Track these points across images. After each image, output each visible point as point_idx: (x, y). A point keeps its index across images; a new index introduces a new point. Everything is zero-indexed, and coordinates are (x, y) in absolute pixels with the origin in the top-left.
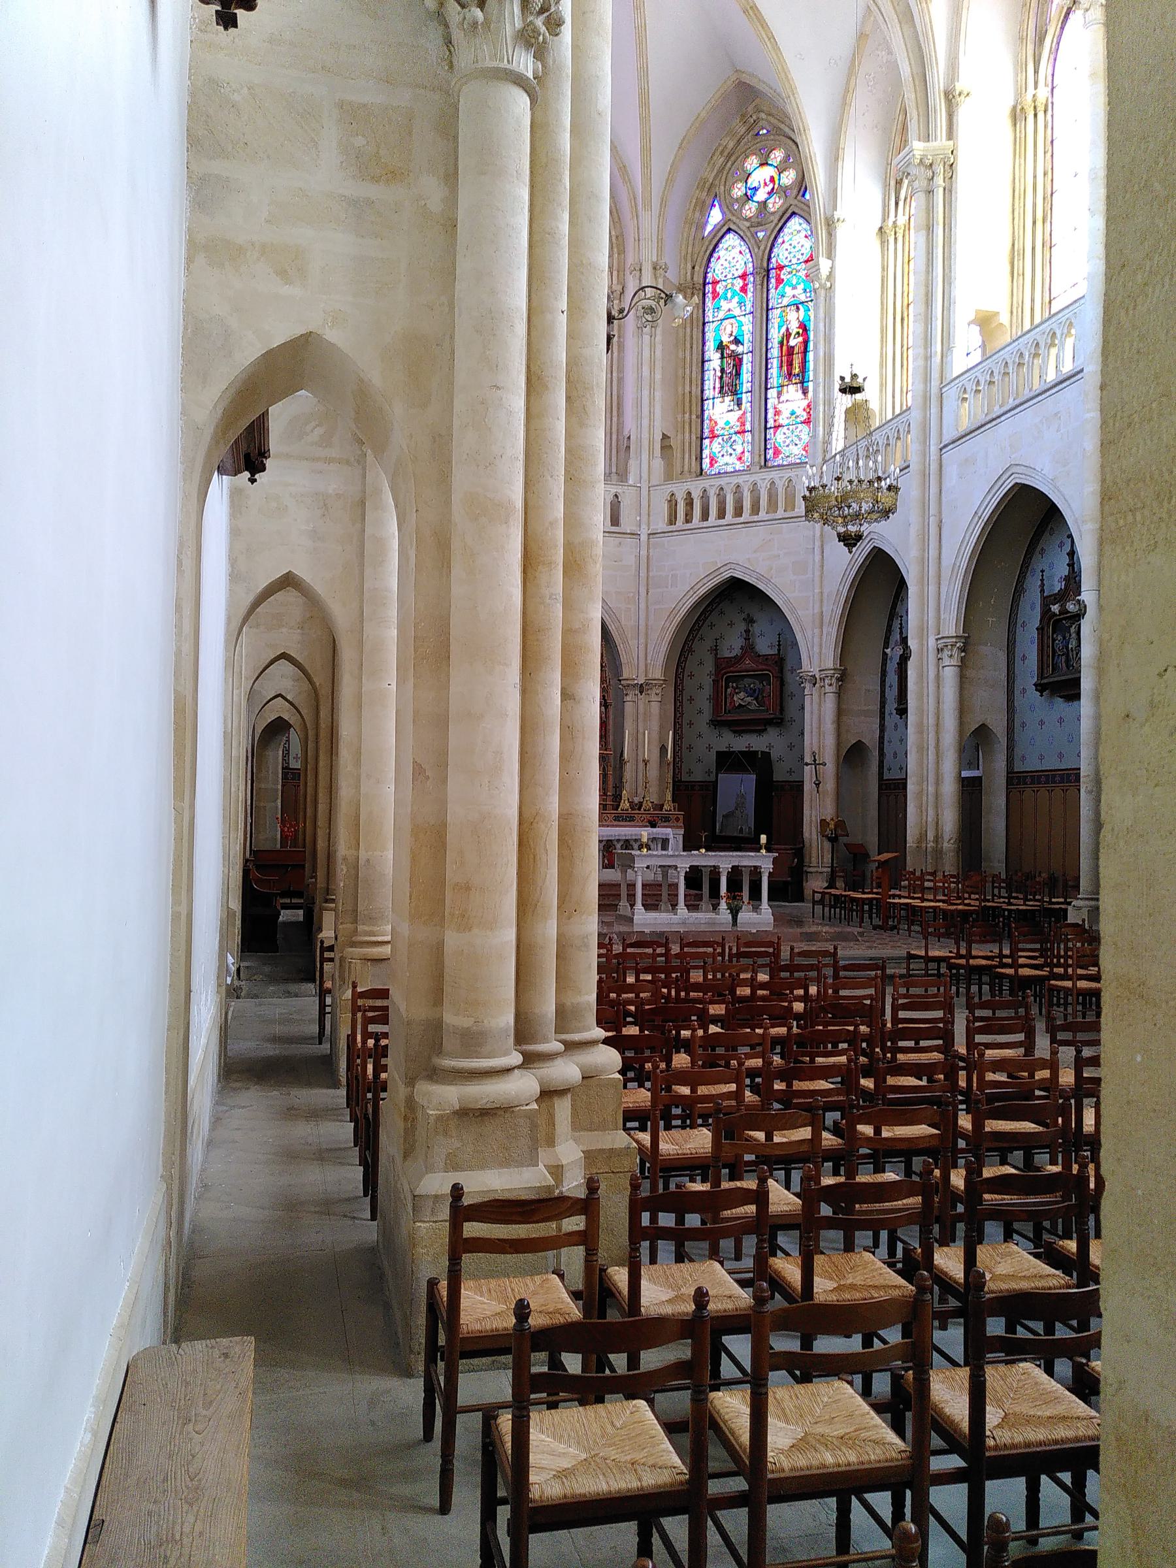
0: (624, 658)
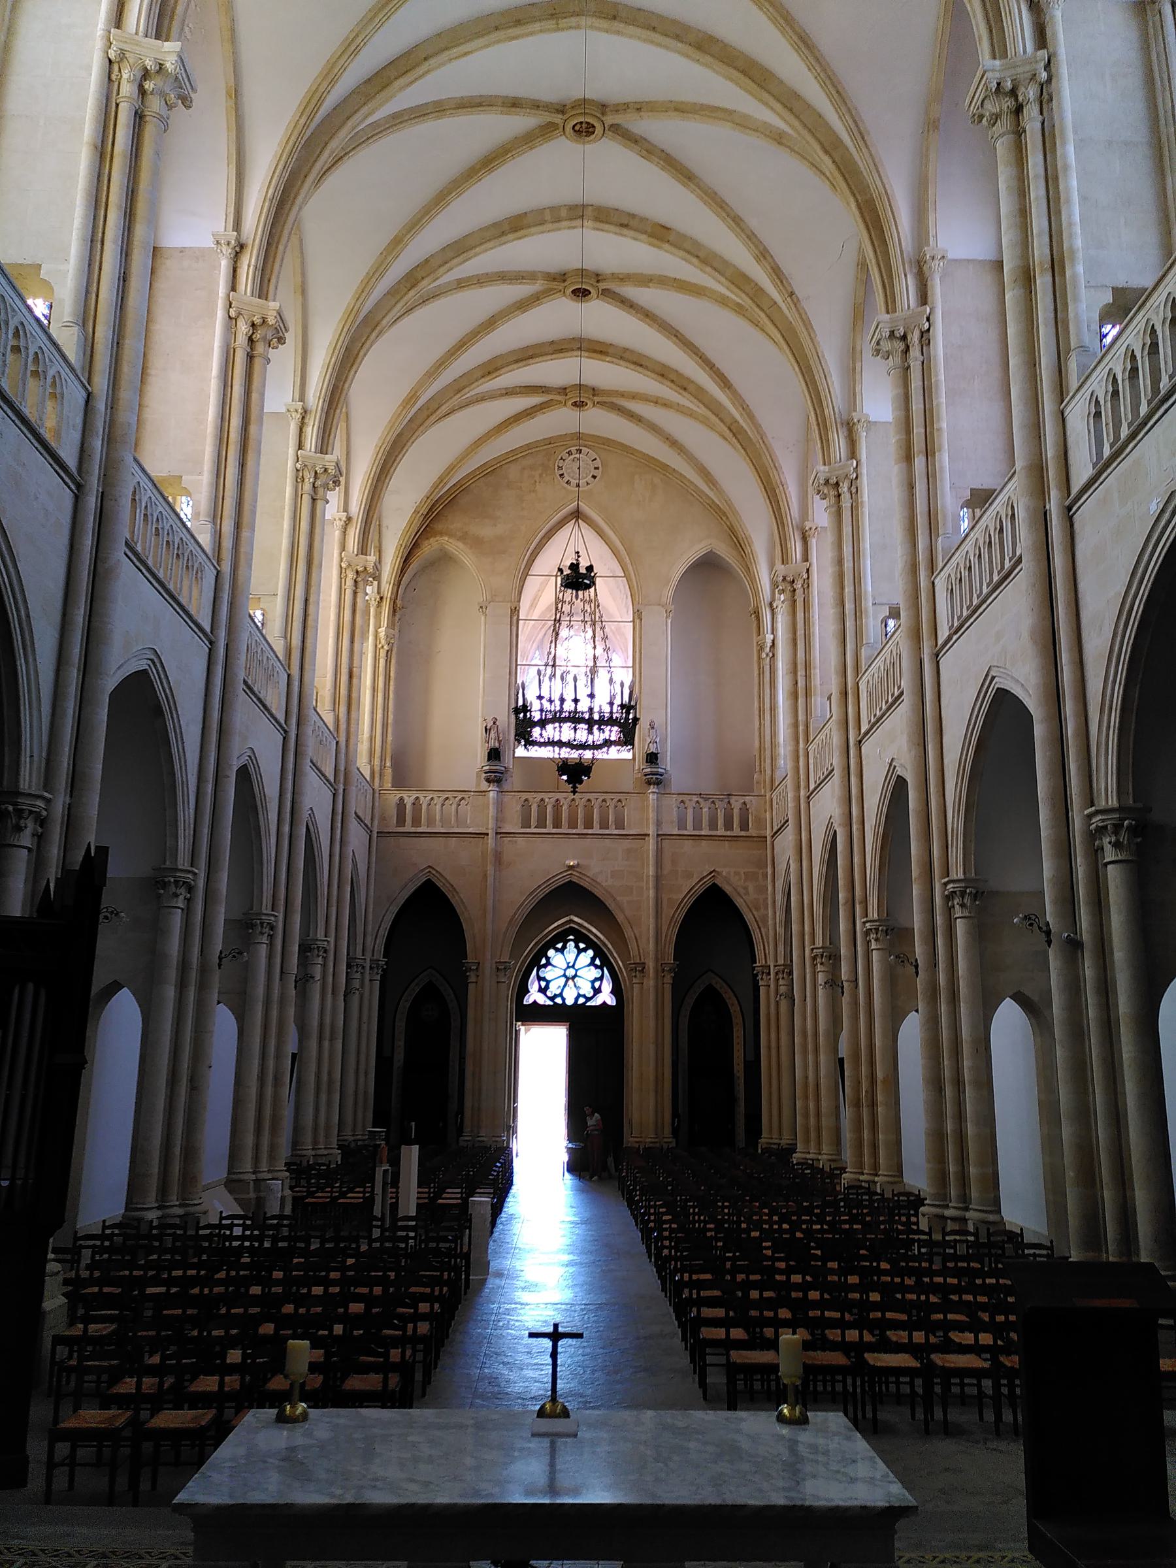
0: (620, 918)
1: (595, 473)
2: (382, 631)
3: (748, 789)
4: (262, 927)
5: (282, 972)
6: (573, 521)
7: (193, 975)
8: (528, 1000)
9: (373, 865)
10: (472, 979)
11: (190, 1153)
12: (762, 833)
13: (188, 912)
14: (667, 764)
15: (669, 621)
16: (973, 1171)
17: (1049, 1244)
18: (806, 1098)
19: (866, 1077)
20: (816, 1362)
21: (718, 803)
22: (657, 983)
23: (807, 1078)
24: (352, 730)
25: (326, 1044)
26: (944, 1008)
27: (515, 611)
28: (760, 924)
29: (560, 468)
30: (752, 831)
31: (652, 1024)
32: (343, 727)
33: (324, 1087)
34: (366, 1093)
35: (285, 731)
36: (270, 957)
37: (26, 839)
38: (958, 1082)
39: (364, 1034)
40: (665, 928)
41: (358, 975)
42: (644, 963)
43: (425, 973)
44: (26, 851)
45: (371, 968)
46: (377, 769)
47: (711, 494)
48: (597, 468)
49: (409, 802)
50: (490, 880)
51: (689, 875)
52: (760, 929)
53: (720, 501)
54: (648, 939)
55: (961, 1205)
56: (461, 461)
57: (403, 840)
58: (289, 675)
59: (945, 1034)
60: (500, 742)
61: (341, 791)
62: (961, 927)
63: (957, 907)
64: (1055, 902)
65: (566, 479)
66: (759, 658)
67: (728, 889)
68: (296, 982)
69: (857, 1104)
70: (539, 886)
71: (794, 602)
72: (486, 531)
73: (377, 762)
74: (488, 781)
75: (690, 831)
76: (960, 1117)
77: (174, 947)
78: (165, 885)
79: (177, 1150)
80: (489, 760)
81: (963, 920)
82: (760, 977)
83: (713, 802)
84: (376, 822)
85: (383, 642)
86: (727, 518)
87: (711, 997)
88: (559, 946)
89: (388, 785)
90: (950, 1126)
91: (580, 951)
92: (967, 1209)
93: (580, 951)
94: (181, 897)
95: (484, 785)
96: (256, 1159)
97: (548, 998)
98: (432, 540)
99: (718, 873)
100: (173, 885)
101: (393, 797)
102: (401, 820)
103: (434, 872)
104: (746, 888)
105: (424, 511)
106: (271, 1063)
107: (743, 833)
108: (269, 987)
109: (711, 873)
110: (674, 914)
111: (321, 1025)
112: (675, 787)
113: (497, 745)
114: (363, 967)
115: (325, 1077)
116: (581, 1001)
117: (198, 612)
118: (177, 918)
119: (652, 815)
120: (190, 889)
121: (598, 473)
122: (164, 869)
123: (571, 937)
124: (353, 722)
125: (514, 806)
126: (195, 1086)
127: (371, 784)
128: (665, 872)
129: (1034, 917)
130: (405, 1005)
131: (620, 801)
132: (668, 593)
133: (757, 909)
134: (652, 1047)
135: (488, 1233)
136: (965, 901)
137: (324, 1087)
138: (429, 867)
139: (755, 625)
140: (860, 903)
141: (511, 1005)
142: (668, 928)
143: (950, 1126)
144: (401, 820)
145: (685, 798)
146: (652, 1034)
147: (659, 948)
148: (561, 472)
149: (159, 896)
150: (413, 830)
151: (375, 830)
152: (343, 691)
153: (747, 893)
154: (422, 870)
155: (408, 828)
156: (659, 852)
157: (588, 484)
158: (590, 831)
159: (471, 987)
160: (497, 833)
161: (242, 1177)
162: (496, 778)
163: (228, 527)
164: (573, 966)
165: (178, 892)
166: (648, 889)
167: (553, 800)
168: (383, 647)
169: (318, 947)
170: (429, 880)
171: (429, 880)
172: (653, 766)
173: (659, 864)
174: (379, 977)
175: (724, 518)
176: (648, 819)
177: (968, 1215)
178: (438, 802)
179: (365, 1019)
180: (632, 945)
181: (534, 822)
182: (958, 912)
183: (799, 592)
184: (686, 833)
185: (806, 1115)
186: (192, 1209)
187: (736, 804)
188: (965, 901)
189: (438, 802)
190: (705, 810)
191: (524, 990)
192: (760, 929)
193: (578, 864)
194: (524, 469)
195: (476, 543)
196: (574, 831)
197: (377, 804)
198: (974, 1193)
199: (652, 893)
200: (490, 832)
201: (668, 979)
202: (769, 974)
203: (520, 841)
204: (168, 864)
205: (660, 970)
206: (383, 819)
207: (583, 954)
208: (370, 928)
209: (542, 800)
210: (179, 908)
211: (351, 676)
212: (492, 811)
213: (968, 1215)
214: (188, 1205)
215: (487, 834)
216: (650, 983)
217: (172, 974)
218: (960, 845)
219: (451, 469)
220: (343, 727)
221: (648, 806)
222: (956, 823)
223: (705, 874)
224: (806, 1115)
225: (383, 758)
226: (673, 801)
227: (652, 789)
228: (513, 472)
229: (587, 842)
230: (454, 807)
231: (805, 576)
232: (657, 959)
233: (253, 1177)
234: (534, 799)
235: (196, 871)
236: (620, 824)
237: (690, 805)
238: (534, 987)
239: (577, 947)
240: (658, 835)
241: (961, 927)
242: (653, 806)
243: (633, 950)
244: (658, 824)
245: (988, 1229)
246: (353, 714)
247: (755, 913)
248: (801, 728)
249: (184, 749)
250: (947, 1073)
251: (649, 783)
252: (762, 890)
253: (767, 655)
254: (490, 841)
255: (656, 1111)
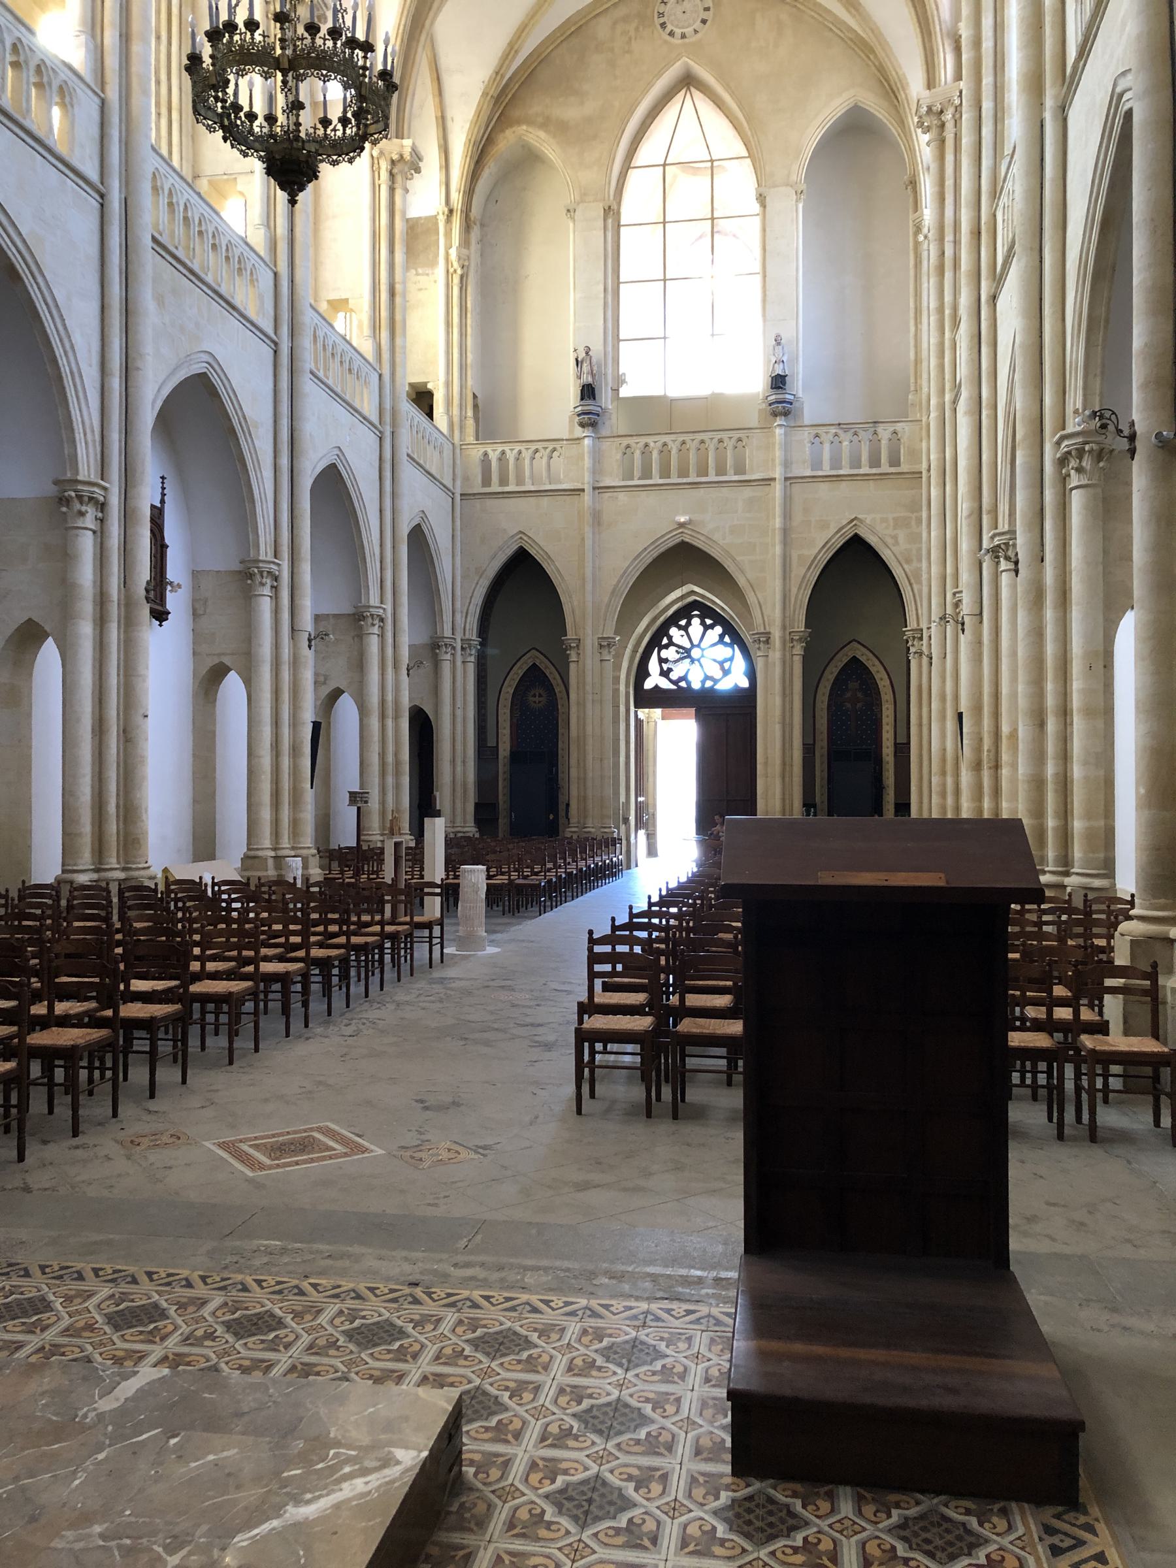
0: (741, 581)
1: (705, 15)
2: (453, 253)
3: (902, 415)
4: (262, 577)
5: (293, 629)
6: (683, 92)
7: (114, 611)
8: (649, 684)
9: (458, 533)
10: (573, 657)
11: (130, 812)
12: (915, 468)
13: (101, 534)
14: (798, 387)
15: (801, 206)
16: (1078, 825)
17: (1129, 899)
18: (943, 773)
19: (989, 732)
20: (704, 1031)
21: (862, 434)
22: (784, 655)
23: (945, 750)
24: (398, 360)
25: (390, 723)
26: (1049, 614)
27: (612, 213)
28: (912, 581)
29: (661, 15)
30: (904, 468)
31: (778, 701)
32: (386, 356)
33: (390, 769)
34: (465, 785)
35: (276, 344)
36: (276, 611)
37: (89, 521)
38: (1065, 712)
39: (459, 720)
40: (794, 590)
41: (448, 657)
42: (769, 633)
43: (528, 655)
44: (90, 533)
45: (463, 649)
46: (456, 419)
47: (852, 22)
48: (707, 9)
49: (493, 456)
50: (588, 543)
51: (824, 525)
52: (911, 584)
53: (864, 31)
54: (774, 605)
55: (1060, 869)
56: (532, 17)
57: (490, 503)
58: (275, 274)
59: (1050, 649)
60: (593, 375)
61: (388, 434)
62: (1077, 500)
63: (1073, 472)
64: (1145, 386)
65: (668, 30)
66: (917, 244)
67: (872, 540)
68: (310, 640)
69: (977, 766)
70: (645, 549)
71: (942, 141)
72: (570, 112)
73: (456, 411)
74: (582, 425)
75: (827, 470)
76: (1065, 756)
77: (86, 574)
78: (67, 501)
79: (112, 808)
80: (582, 399)
81: (1079, 490)
82: (910, 643)
83: (855, 434)
84: (458, 483)
85: (456, 265)
86: (876, 56)
87: (855, 668)
88: (683, 623)
89: (471, 439)
90: (1051, 769)
91: (707, 628)
92: (1067, 874)
93: (707, 628)
94: (377, 626)
95: (579, 432)
96: (276, 834)
97: (671, 681)
98: (509, 133)
99: (861, 521)
100: (76, 500)
101: (476, 453)
102: (487, 481)
103: (525, 538)
104: (895, 538)
105: (493, 92)
106: (286, 731)
107: (893, 470)
108: (277, 645)
109: (852, 521)
110: (805, 575)
111: (383, 702)
112: (808, 417)
113: (590, 380)
114: (454, 648)
115: (390, 758)
116: (709, 684)
117: (72, 150)
118: (86, 544)
119: (778, 454)
120: (102, 506)
121: (708, 15)
122: (64, 481)
123: (696, 612)
124: (398, 350)
125: (613, 453)
126: (128, 737)
127: (450, 438)
128: (795, 524)
129: (1107, 414)
130: (509, 690)
131: (740, 440)
132: (798, 170)
133: (908, 561)
134: (778, 728)
135: (257, 860)
136: (1084, 464)
137: (390, 769)
138: (521, 532)
139: (911, 200)
140: (989, 512)
141: (625, 688)
142: (799, 588)
143: (1051, 769)
144: (487, 481)
145: (821, 430)
146: (778, 712)
147: (787, 615)
148: (662, 20)
149: (437, 654)
150: (500, 489)
151: (458, 492)
152: (384, 314)
153: (897, 543)
154: (513, 536)
155: (495, 487)
156: (787, 500)
157: (696, 32)
158: (703, 479)
159: (572, 666)
160: (594, 488)
161: (260, 853)
162: (590, 420)
163: (111, 38)
164: (698, 646)
165: (84, 508)
166: (774, 546)
167: (659, 444)
168: (455, 271)
169: (372, 615)
170: (521, 548)
171: (521, 548)
172: (780, 391)
173: (787, 515)
174: (472, 659)
175: (871, 57)
176: (773, 460)
177: (1067, 881)
178: (526, 455)
179: (459, 704)
180: (756, 613)
181: (637, 473)
182: (1075, 480)
183: (950, 126)
184: (820, 473)
185: (943, 795)
186: (136, 874)
187: (884, 433)
188: (1084, 464)
189: (526, 455)
190: (845, 443)
191: (642, 672)
192: (911, 584)
193: (690, 520)
194: (615, 23)
195: (559, 129)
196: (685, 480)
197: (458, 462)
198: (1077, 853)
199: (778, 550)
200: (586, 487)
201: (798, 650)
202: (921, 639)
203: (622, 497)
204: (69, 475)
205: (789, 639)
206: (466, 479)
207: (710, 631)
208: (458, 605)
209: (646, 445)
210: (86, 529)
211: (392, 293)
212: (587, 462)
213: (1067, 881)
214: (130, 869)
215: (583, 490)
216: (776, 655)
217: (87, 607)
218: (1080, 383)
219: (523, 30)
220: (386, 356)
221: (774, 444)
222: (1076, 353)
223: (845, 522)
224: (943, 795)
225: (462, 406)
226: (805, 435)
227: (780, 421)
228: (602, 28)
229: (701, 493)
230: (545, 459)
231: (957, 102)
232: (784, 628)
233: (273, 854)
234: (637, 443)
235: (107, 485)
236: (740, 469)
237: (827, 438)
238: (653, 666)
239: (703, 623)
240: (786, 479)
241: (1077, 500)
242: (780, 444)
243: (758, 619)
244: (787, 464)
245: (1086, 895)
246: (399, 341)
247: (906, 566)
248: (947, 312)
249: (65, 328)
250: (1051, 701)
251: (775, 414)
252: (915, 538)
253: (926, 237)
254: (587, 497)
255: (783, 800)
